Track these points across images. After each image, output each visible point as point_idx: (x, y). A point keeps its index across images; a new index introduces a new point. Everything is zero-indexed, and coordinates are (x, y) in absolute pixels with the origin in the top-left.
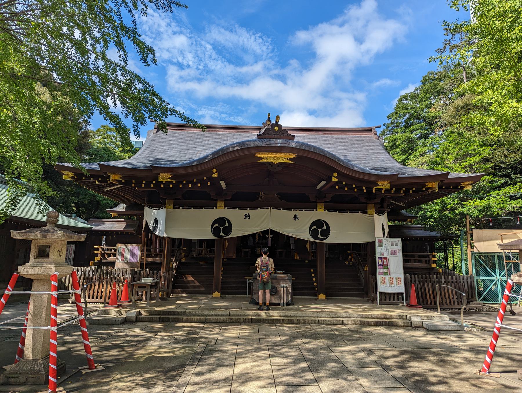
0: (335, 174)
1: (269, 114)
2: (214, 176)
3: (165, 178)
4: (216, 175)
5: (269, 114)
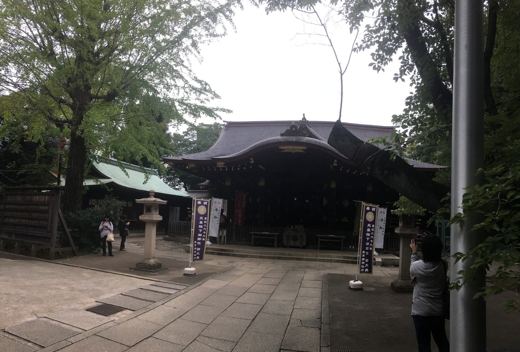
0: (336, 161)
1: (304, 114)
2: (251, 162)
3: (220, 165)
4: (252, 162)
5: (304, 114)
